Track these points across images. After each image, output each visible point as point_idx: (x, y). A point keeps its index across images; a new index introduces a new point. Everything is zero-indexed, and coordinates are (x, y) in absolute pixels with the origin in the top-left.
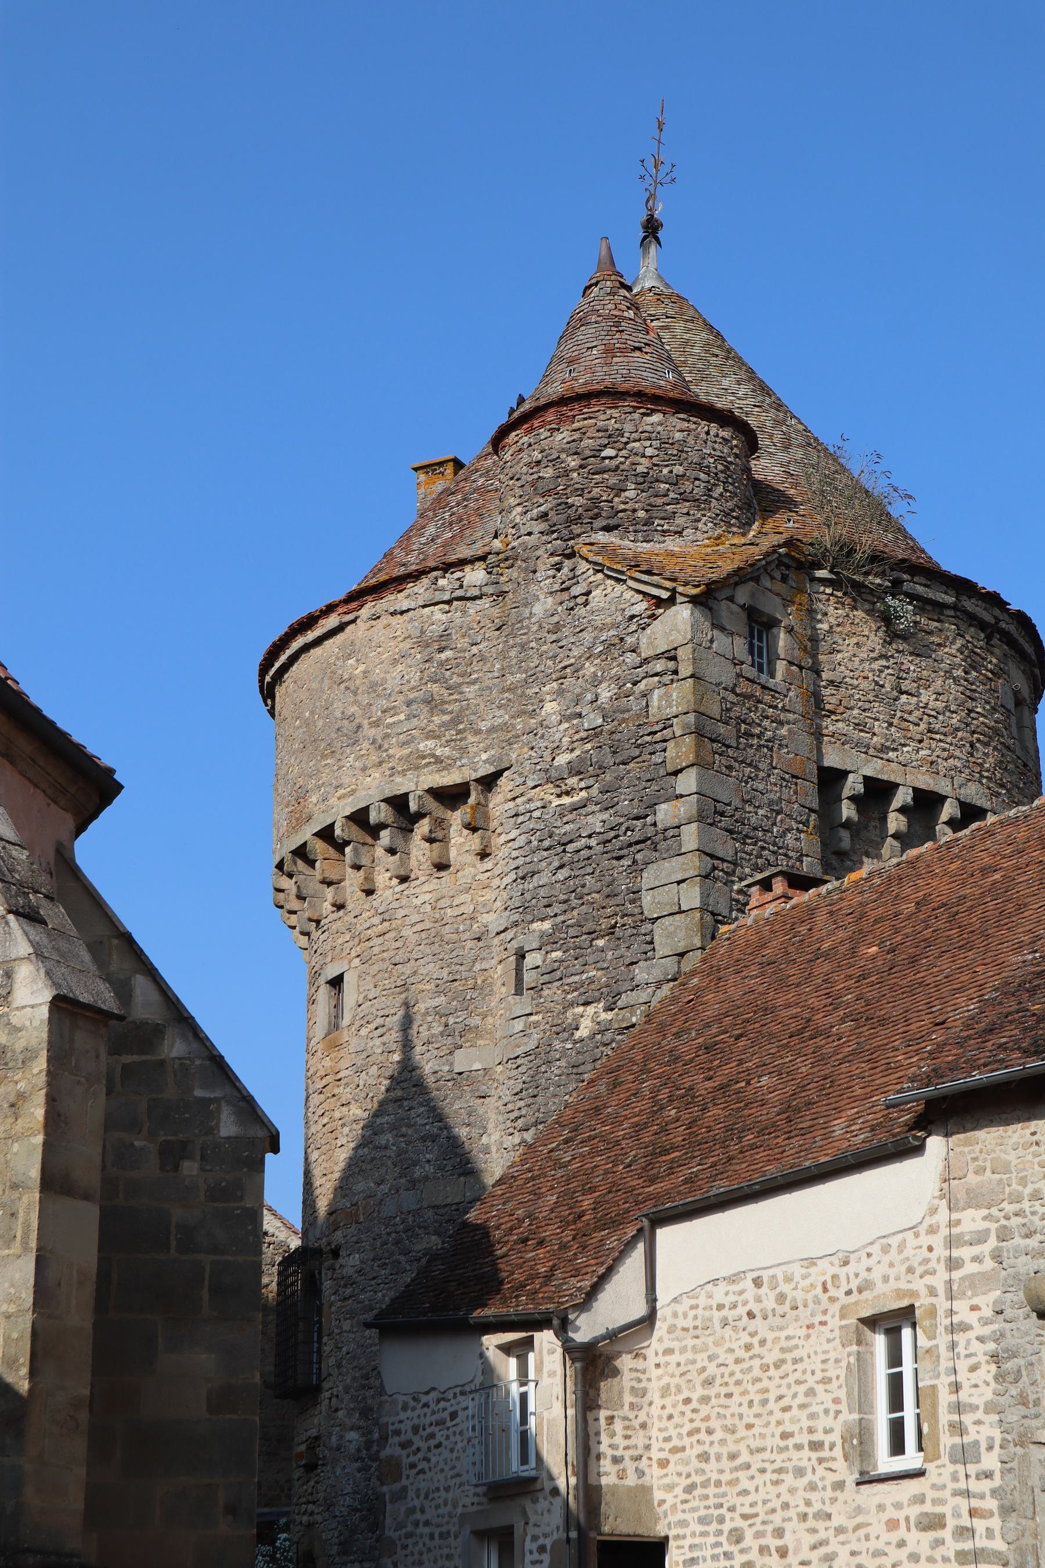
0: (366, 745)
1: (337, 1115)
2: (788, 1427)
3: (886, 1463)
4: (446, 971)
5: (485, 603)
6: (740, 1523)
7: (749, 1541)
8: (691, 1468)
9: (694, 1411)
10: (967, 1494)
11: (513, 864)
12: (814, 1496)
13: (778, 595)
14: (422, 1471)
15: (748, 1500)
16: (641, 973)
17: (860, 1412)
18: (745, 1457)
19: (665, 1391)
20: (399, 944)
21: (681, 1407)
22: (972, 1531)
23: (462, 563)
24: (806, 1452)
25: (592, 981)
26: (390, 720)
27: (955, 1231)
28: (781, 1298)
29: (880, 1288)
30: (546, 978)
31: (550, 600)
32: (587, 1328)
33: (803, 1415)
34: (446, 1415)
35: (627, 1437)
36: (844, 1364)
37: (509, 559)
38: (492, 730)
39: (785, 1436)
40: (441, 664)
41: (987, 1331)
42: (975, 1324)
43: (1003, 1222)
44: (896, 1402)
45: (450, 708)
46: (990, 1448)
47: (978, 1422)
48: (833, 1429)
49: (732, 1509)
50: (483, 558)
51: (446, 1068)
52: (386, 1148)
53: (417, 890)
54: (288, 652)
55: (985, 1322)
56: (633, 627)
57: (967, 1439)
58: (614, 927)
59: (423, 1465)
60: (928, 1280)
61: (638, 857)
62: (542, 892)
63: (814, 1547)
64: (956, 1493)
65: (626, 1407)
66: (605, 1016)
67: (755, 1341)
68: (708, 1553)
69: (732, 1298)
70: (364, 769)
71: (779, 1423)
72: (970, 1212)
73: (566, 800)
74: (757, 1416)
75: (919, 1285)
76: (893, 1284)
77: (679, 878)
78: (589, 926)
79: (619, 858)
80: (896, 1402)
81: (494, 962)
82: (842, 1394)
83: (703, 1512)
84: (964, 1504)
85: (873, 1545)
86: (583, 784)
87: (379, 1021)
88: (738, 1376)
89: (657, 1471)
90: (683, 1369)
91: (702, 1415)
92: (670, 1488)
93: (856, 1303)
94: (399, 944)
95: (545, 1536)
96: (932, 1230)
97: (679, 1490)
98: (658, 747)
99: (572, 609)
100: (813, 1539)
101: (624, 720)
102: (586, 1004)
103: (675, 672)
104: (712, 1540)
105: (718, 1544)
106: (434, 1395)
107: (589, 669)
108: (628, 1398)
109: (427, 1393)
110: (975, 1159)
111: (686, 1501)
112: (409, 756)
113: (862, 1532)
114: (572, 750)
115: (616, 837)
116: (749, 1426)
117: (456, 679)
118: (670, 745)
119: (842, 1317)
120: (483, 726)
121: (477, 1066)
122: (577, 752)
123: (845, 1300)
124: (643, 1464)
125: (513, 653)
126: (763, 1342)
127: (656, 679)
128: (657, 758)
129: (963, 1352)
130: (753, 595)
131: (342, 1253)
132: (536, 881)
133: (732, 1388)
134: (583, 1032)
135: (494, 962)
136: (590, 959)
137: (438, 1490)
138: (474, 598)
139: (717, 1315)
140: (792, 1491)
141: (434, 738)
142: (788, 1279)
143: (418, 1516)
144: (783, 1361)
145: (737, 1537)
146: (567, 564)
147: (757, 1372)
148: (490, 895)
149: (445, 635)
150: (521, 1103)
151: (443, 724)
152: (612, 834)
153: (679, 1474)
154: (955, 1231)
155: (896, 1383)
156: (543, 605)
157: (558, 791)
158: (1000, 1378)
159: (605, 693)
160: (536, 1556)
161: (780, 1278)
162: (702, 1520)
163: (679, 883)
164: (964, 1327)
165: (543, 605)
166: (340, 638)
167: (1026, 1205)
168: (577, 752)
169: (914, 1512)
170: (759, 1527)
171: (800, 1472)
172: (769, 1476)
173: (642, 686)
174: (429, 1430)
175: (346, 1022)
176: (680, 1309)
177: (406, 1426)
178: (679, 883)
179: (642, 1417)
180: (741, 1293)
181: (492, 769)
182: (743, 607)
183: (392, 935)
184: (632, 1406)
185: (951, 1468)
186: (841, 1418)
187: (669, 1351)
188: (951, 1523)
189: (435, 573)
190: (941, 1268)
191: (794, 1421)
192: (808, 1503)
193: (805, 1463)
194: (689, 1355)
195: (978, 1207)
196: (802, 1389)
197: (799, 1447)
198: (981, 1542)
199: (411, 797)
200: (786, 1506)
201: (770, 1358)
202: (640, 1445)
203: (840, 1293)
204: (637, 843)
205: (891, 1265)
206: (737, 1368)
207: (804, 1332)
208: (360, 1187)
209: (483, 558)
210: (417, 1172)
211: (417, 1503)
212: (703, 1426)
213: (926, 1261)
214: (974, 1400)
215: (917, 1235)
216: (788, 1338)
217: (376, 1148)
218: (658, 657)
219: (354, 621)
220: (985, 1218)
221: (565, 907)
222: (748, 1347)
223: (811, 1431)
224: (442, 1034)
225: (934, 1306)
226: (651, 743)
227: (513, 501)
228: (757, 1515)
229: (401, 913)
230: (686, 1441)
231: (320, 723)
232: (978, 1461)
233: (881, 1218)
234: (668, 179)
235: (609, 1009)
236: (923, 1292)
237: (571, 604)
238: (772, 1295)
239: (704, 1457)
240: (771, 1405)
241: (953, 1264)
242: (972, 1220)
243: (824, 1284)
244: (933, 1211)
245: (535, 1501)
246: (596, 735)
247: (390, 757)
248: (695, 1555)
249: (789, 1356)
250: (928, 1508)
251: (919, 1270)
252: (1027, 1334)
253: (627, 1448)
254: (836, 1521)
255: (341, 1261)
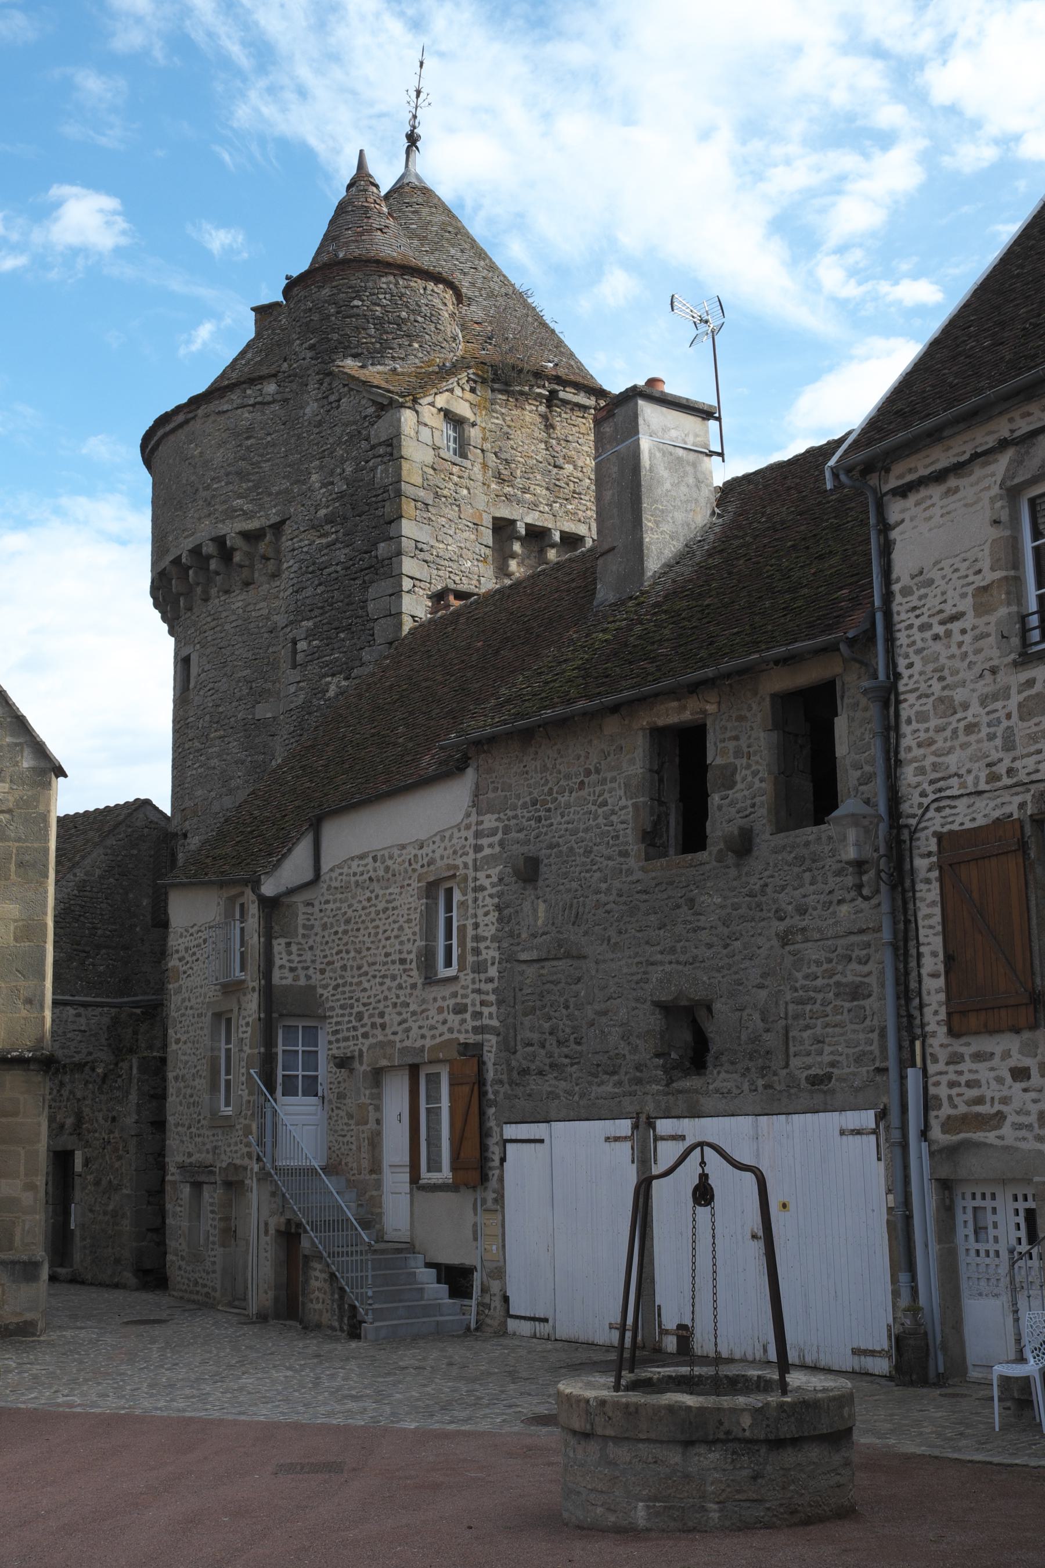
0: (201, 502)
1: (186, 746)
2: (388, 950)
3: (443, 972)
4: (251, 653)
5: (276, 407)
6: (362, 1009)
7: (366, 1020)
8: (337, 975)
9: (340, 939)
10: (479, 991)
11: (291, 583)
12: (401, 992)
13: (466, 401)
14: (189, 976)
15: (366, 994)
16: (366, 655)
17: (426, 940)
18: (365, 968)
19: (324, 927)
20: (223, 635)
21: (333, 937)
22: (481, 1014)
23: (262, 378)
24: (397, 966)
25: (337, 660)
26: (215, 486)
27: (480, 828)
28: (387, 869)
29: (439, 863)
30: (309, 658)
31: (316, 404)
32: (269, 888)
33: (397, 942)
34: (201, 941)
35: (300, 955)
36: (419, 911)
37: (292, 376)
38: (277, 494)
39: (387, 955)
40: (248, 448)
41: (494, 890)
42: (488, 887)
43: (506, 822)
44: (449, 936)
45: (253, 478)
46: (493, 964)
47: (487, 948)
48: (413, 949)
49: (358, 1000)
50: (275, 375)
51: (250, 717)
52: (214, 768)
53: (234, 600)
54: (156, 438)
55: (493, 885)
56: (367, 424)
57: (481, 958)
58: (351, 624)
59: (190, 972)
60: (464, 859)
61: (366, 578)
62: (308, 601)
63: (400, 1024)
64: (473, 992)
65: (300, 936)
66: (344, 683)
67: (373, 895)
68: (345, 1027)
69: (361, 869)
70: (199, 519)
71: (384, 947)
72: (488, 816)
73: (324, 541)
74: (372, 942)
75: (459, 862)
76: (446, 861)
77: (390, 592)
78: (336, 624)
79: (354, 579)
80: (449, 936)
81: (280, 647)
82: (417, 929)
83: (342, 1002)
84: (478, 998)
85: (431, 1022)
86: (333, 530)
87: (211, 685)
88: (364, 918)
89: (319, 976)
90: (334, 913)
91: (344, 941)
92: (325, 987)
93: (426, 873)
94: (223, 635)
95: (249, 1016)
96: (468, 827)
97: (330, 988)
98: (380, 505)
99: (329, 411)
100: (399, 1019)
101: (360, 486)
102: (333, 675)
103: (391, 454)
104: (346, 1019)
105: (350, 1022)
106: (196, 928)
107: (339, 452)
108: (301, 931)
109: (192, 927)
110: (493, 782)
111: (333, 995)
112: (227, 510)
113: (425, 1015)
114: (328, 507)
115: (354, 565)
116: (368, 949)
117: (257, 458)
118: (387, 504)
119: (419, 881)
120: (275, 489)
121: (269, 715)
122: (331, 508)
123: (420, 871)
124: (311, 971)
125: (292, 441)
126: (377, 897)
127: (380, 459)
128: (379, 513)
129: (481, 904)
130: (448, 402)
131: (189, 835)
132: (304, 594)
133: (360, 925)
134: (331, 693)
135: (280, 647)
136: (336, 646)
137: (196, 987)
138: (269, 403)
139: (353, 879)
140: (389, 989)
141: (242, 498)
142: (391, 857)
143: (187, 1003)
144: (387, 909)
145: (360, 1016)
146: (327, 380)
147: (373, 915)
148: (277, 603)
149: (250, 429)
150: (293, 740)
151: (248, 489)
152: (351, 563)
153: (331, 978)
154: (480, 828)
155: (449, 921)
156: (311, 409)
157: (318, 534)
158: (500, 920)
159: (349, 469)
160: (244, 1029)
161: (387, 855)
162: (342, 1007)
163: (390, 595)
164: (482, 888)
165: (311, 409)
166: (187, 429)
167: (519, 812)
168: (331, 508)
169: (451, 1002)
170: (371, 1011)
171: (394, 978)
172: (378, 980)
173: (371, 464)
174: (193, 950)
175: (192, 686)
176: (334, 875)
177: (182, 948)
178: (390, 595)
179: (311, 942)
180: (366, 865)
181: (278, 519)
182: (440, 410)
183: (219, 628)
184: (304, 936)
185: (471, 976)
186: (417, 944)
187: (327, 902)
188: (470, 1009)
189: (244, 386)
190: (471, 851)
191: (392, 946)
192: (398, 997)
193: (396, 972)
194: (338, 905)
195: (493, 813)
196: (396, 926)
197: (393, 962)
198: (486, 1021)
199: (228, 538)
200: (386, 998)
201: (381, 906)
202: (309, 960)
203: (418, 867)
204: (366, 569)
205: (445, 849)
206: (362, 913)
207: (398, 890)
208: (199, 793)
209: (275, 375)
210: (233, 784)
211: (186, 995)
212: (344, 948)
213: (464, 846)
214: (486, 934)
215: (459, 830)
216: (390, 894)
217: (208, 768)
218: (380, 444)
219: (193, 418)
220: (496, 820)
221: (321, 611)
222: (369, 899)
223: (400, 952)
224: (248, 694)
225: (466, 875)
226: (376, 503)
227: (294, 336)
228: (370, 1004)
229: (224, 614)
230: (335, 958)
231: (174, 487)
232: (486, 972)
233: (433, 820)
234: (426, 103)
235: (346, 679)
236: (461, 866)
237: (329, 408)
238: (382, 868)
239: (344, 968)
240: (380, 936)
241: (478, 849)
242: (490, 821)
243: (410, 860)
244: (468, 815)
245: (245, 995)
246: (342, 497)
247: (215, 510)
248: (338, 1028)
249: (390, 905)
250: (459, 1000)
251: (460, 852)
252: (515, 893)
253: (299, 962)
254: (413, 1007)
255: (188, 840)
